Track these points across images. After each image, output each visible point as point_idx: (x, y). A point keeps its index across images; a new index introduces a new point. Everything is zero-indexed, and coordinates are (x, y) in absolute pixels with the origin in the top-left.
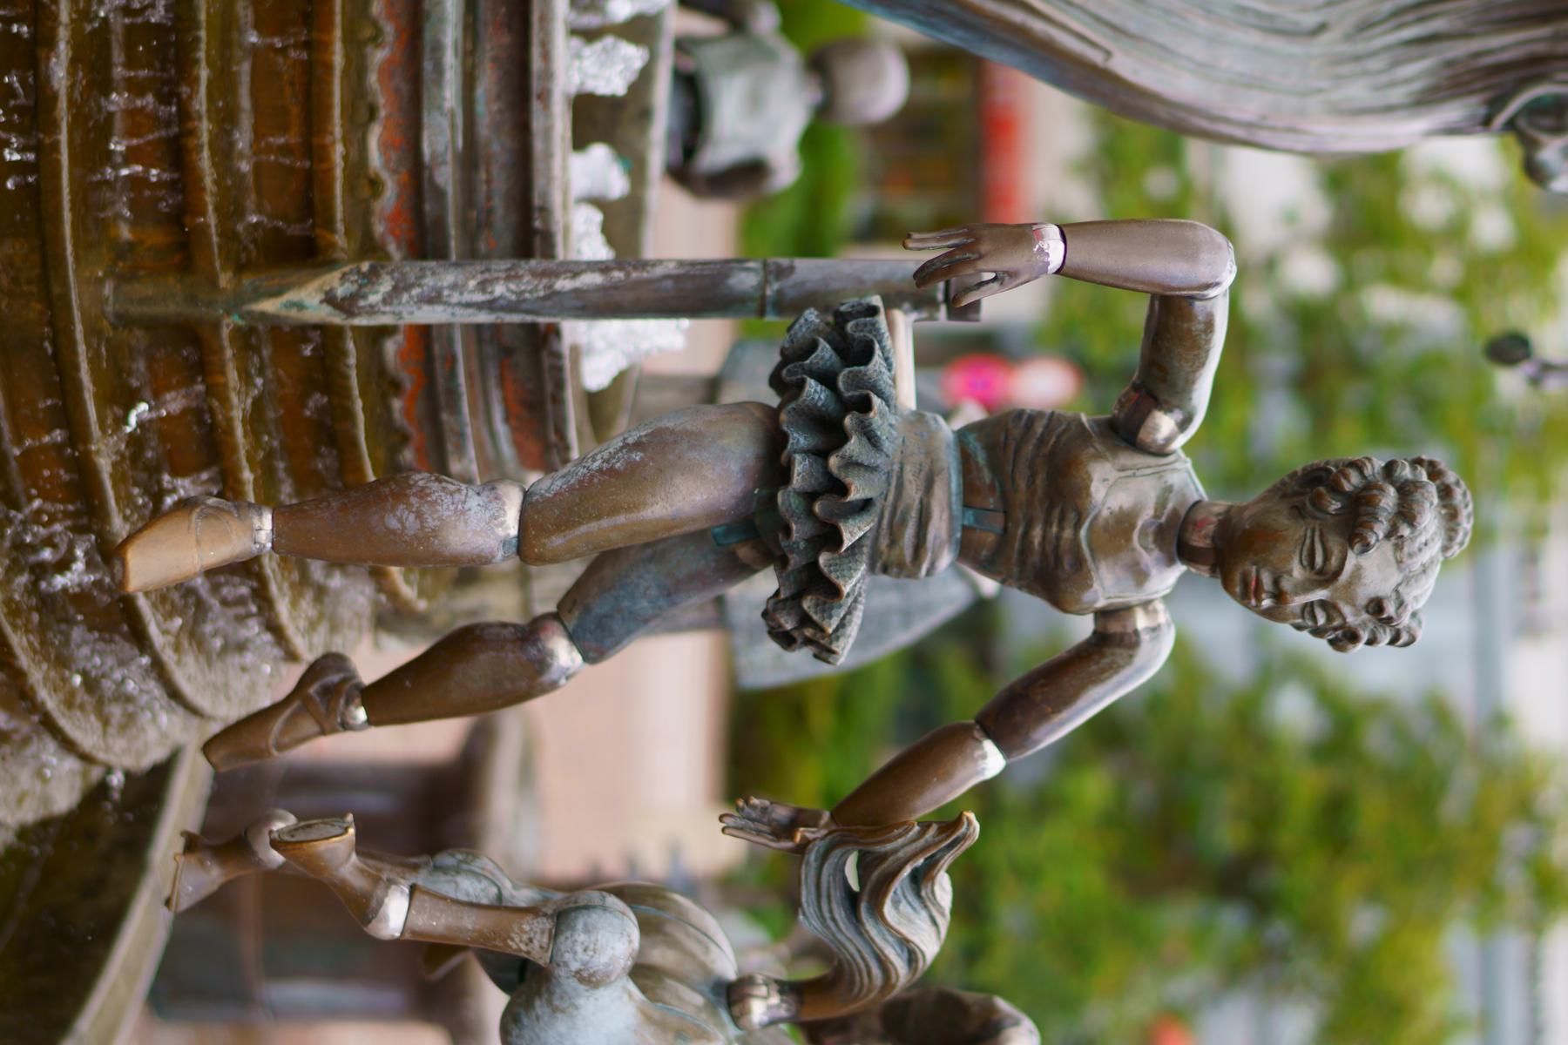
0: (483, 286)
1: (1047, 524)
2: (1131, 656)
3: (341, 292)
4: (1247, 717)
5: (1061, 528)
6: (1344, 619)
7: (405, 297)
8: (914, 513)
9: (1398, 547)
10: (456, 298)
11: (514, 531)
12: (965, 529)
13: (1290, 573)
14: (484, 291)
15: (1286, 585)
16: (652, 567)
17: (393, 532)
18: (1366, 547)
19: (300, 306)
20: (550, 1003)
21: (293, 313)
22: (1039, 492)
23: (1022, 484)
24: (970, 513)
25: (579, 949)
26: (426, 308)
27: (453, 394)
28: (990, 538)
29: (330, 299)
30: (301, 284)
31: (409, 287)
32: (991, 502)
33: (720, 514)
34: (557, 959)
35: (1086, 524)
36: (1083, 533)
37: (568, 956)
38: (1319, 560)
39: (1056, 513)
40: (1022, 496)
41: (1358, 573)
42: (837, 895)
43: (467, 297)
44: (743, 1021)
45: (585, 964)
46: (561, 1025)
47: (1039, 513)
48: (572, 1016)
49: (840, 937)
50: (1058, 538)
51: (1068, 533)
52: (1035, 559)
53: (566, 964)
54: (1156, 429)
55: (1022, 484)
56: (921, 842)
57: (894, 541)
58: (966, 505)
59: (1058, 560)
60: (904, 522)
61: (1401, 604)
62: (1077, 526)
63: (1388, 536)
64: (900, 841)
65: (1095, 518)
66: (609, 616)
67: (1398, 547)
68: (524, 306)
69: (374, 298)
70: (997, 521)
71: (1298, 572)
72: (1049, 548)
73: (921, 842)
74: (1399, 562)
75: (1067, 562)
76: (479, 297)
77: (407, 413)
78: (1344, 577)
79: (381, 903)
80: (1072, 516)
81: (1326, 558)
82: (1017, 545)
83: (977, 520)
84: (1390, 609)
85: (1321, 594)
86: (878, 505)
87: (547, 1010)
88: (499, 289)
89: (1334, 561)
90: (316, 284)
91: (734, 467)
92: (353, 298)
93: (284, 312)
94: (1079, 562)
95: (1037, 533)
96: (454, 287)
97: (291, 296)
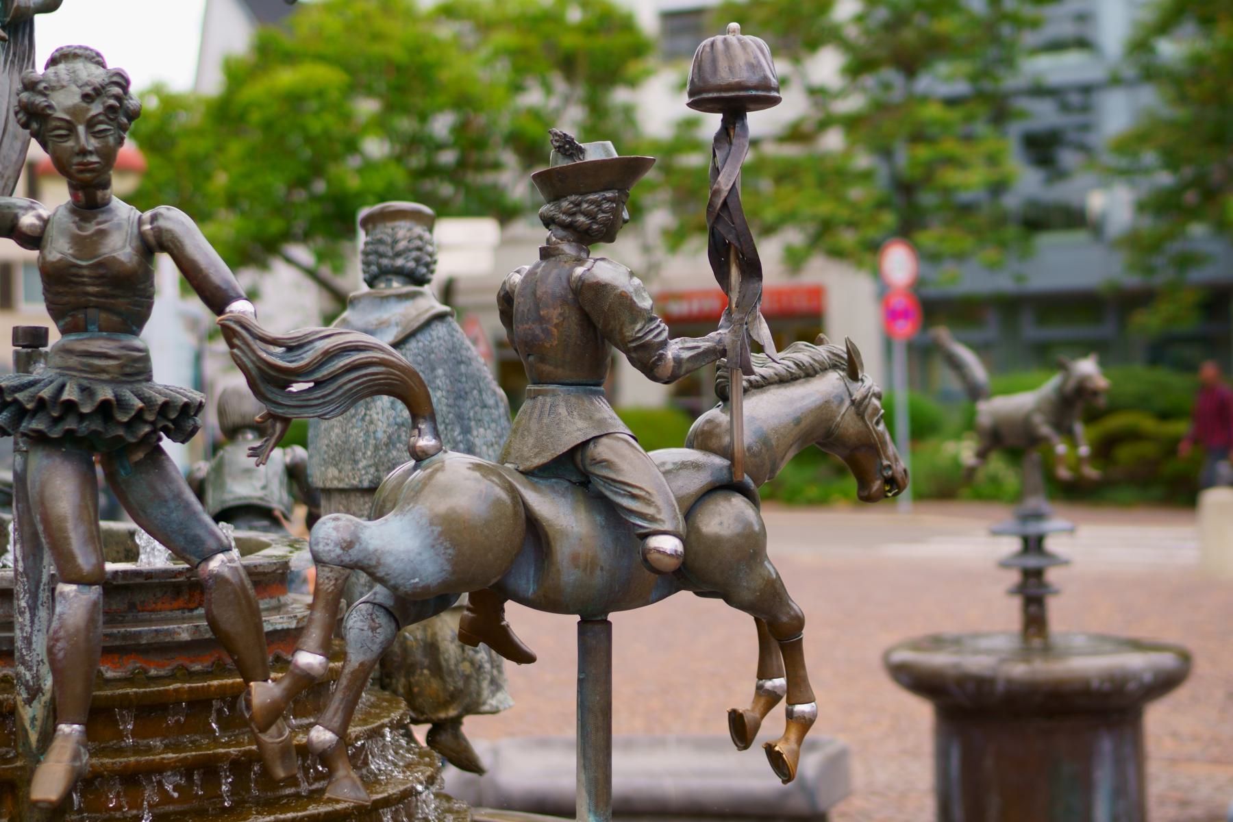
0: (22, 613)
1: (84, 284)
2: (167, 230)
3: (25, 696)
4: (1178, 82)
5: (83, 276)
6: (99, 114)
7: (27, 658)
8: (85, 360)
9: (53, 89)
10: (28, 629)
11: (74, 587)
12: (101, 330)
13: (72, 147)
14: (24, 613)
15: (77, 149)
16: (149, 511)
17: (65, 655)
18: (50, 107)
19: (34, 719)
20: (375, 567)
21: (38, 723)
22: (66, 289)
23: (65, 299)
24: (90, 328)
25: (327, 548)
26: (34, 646)
27: (125, 636)
28: (103, 315)
29: (29, 702)
30: (21, 718)
31: (22, 656)
32: (81, 316)
33: (552, 488)
34: (337, 561)
35: (79, 262)
36: (84, 263)
37: (333, 555)
38: (63, 132)
39: (75, 279)
40: (71, 299)
41: (67, 110)
42: (318, 393)
43: (27, 622)
44: (432, 452)
45: (336, 545)
46: (389, 560)
47: (80, 288)
48: (383, 553)
49: (339, 392)
50: (90, 277)
51: (85, 272)
52: (107, 289)
53: (339, 556)
54: (32, 225)
55: (65, 299)
56: (244, 347)
57: (102, 370)
58: (85, 330)
59: (102, 276)
60: (90, 365)
61: (86, 84)
62: (80, 267)
63: (46, 95)
64: (245, 359)
65: (74, 256)
66: (185, 536)
67: (53, 89)
68: (33, 589)
69: (28, 676)
70: (92, 312)
71: (70, 143)
72: (98, 282)
73: (244, 347)
74: (63, 87)
75: (101, 271)
76: (27, 615)
77: (159, 666)
78: (68, 118)
79: (302, 670)
80: (74, 270)
81: (59, 128)
82: (103, 300)
83: (94, 324)
84: (88, 90)
85: (81, 129)
86: (85, 383)
87: (381, 569)
88: (23, 604)
89: (58, 124)
90: (21, 709)
91: (45, 462)
92: (28, 688)
93: (38, 729)
94: (100, 265)
95: (90, 289)
96: (22, 629)
97: (27, 724)
